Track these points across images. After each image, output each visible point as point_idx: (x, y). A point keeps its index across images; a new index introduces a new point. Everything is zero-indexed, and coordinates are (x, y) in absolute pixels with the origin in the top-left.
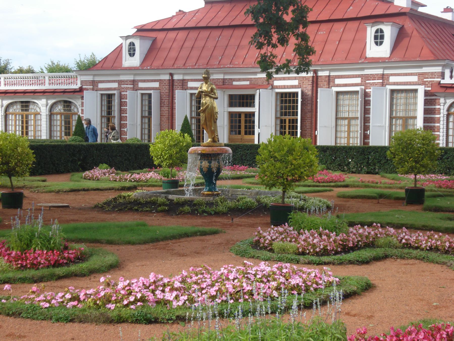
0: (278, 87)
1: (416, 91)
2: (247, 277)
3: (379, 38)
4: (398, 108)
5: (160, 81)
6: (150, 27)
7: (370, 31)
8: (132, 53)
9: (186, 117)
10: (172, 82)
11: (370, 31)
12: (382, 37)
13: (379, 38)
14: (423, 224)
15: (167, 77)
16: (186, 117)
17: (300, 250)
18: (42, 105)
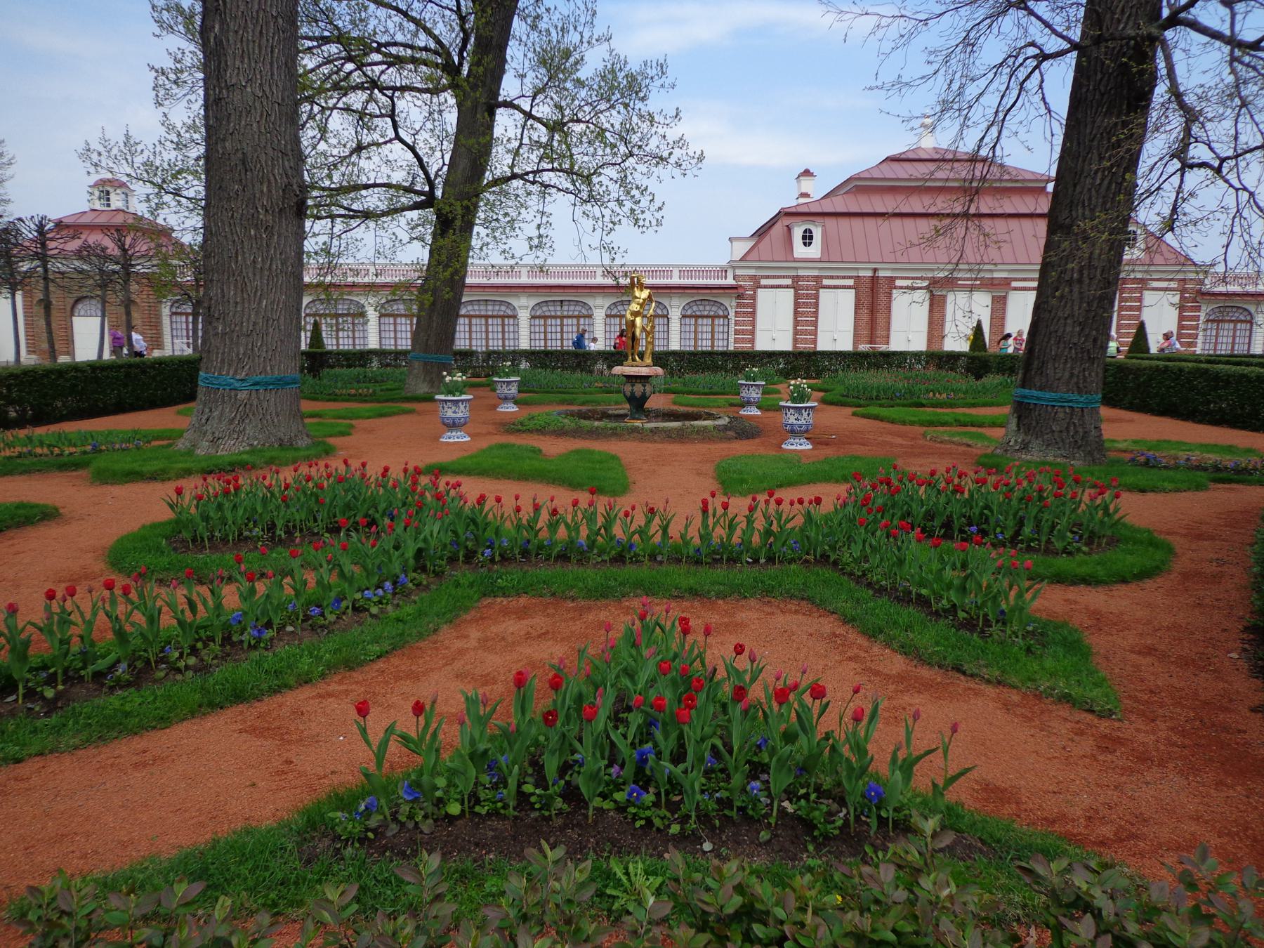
2: (179, 202)
3: (808, 239)
4: (184, 326)
5: (857, 278)
6: (794, 210)
7: (798, 233)
9: (978, 329)
10: (874, 280)
11: (798, 233)
12: (811, 238)
13: (808, 239)
14: (17, 500)
15: (870, 274)
16: (978, 329)
17: (21, 930)
18: (600, 307)
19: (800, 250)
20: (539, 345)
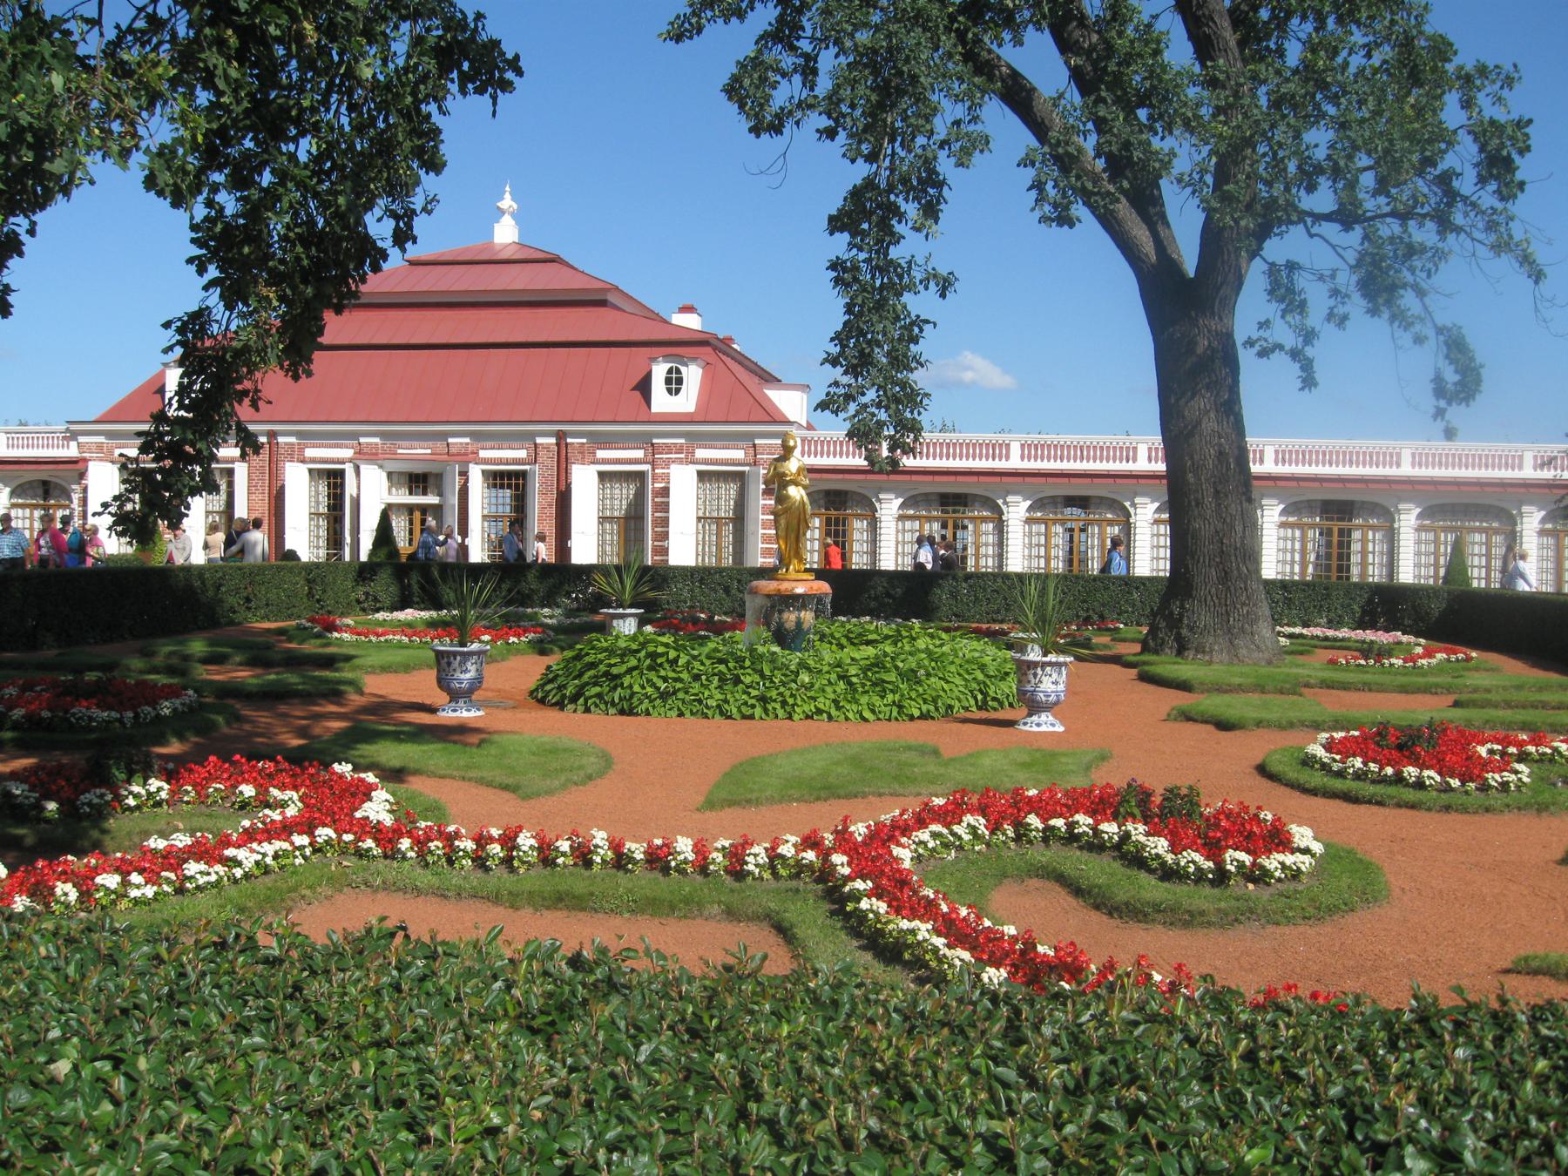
0: (313, 461)
1: (743, 473)
19: (661, 401)
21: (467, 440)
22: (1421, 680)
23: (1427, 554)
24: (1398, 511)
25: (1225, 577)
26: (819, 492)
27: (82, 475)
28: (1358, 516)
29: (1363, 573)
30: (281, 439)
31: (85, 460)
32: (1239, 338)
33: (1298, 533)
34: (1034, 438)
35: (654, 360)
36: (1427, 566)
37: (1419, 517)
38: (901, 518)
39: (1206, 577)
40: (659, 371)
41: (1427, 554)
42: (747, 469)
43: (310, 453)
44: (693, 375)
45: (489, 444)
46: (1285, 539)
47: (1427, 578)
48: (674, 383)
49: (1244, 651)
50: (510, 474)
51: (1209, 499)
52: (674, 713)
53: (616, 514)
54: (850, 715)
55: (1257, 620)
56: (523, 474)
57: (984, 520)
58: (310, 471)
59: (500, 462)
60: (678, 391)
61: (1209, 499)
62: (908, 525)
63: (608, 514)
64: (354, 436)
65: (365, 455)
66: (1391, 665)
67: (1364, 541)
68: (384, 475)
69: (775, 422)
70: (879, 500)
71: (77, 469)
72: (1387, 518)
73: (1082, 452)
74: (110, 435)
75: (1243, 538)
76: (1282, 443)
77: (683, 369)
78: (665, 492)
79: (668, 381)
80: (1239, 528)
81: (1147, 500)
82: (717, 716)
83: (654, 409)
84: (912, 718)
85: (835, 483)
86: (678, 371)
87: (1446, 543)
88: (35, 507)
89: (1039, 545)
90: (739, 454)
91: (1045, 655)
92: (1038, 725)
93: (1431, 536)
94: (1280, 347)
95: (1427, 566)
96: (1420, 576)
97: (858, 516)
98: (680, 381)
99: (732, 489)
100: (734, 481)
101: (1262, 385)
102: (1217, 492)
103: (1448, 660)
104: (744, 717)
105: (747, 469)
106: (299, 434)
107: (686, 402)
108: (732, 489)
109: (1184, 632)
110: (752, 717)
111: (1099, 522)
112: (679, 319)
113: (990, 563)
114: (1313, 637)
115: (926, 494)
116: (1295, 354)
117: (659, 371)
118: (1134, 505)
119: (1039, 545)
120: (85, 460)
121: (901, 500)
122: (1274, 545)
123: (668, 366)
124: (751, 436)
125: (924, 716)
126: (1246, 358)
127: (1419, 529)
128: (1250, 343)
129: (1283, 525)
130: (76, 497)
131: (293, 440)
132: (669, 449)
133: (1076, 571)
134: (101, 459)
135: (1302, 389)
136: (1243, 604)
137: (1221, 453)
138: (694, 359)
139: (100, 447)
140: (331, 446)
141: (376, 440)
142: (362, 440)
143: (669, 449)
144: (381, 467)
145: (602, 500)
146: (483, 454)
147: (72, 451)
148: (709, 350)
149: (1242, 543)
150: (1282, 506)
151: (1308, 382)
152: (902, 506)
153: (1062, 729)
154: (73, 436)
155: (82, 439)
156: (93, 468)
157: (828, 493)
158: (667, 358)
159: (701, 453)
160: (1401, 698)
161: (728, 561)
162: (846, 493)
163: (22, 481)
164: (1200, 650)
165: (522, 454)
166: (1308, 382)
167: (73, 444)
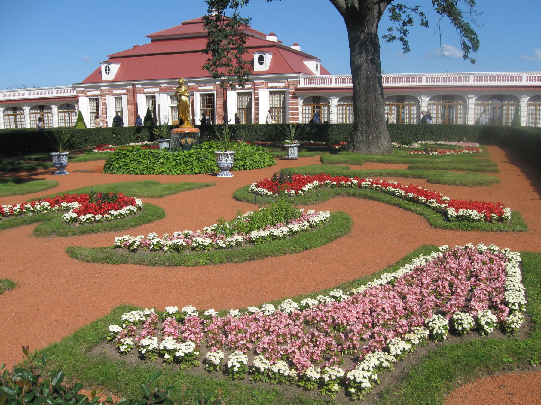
0: (147, 93)
1: (284, 91)
8: (108, 71)
20: (342, 121)
21: (194, 84)
22: (411, 159)
23: (532, 114)
24: (521, 98)
25: (368, 123)
26: (310, 97)
27: (78, 101)
28: (506, 100)
29: (507, 122)
30: (137, 86)
31: (78, 96)
32: (380, 35)
33: (482, 107)
34: (338, 76)
35: (254, 53)
36: (532, 119)
37: (529, 100)
38: (339, 105)
39: (362, 122)
40: (256, 57)
41: (532, 114)
42: (286, 90)
43: (146, 90)
44: (268, 58)
45: (201, 85)
46: (478, 109)
47: (532, 123)
48: (261, 61)
49: (373, 150)
50: (209, 95)
51: (363, 95)
52: (121, 173)
53: (244, 107)
54: (173, 173)
55: (380, 138)
56: (213, 95)
57: (413, 105)
58: (147, 96)
59: (205, 91)
60: (263, 63)
61: (363, 95)
62: (341, 107)
63: (241, 107)
64: (159, 84)
65: (162, 91)
66: (433, 154)
67: (508, 110)
68: (169, 97)
69: (295, 73)
70: (330, 99)
71: (75, 99)
72: (517, 100)
73: (405, 79)
74: (85, 88)
75: (375, 109)
76: (396, 72)
77: (264, 56)
78: (257, 99)
79: (259, 60)
80: (374, 105)
81: (426, 96)
82: (134, 174)
83: (255, 70)
84: (196, 174)
85: (315, 94)
86: (262, 57)
87: (512, 110)
88: (66, 112)
89: (343, 114)
90: (283, 85)
91: (226, 151)
92: (222, 175)
93: (534, 107)
94: (395, 38)
95: (532, 119)
96: (529, 123)
97: (323, 105)
98: (263, 60)
99: (282, 96)
100: (282, 94)
101: (389, 52)
102: (366, 92)
103: (469, 153)
104: (141, 174)
105: (286, 90)
106: (142, 84)
107: (265, 67)
108: (282, 96)
109: (355, 143)
110: (143, 174)
111: (409, 105)
112: (269, 38)
113: (415, 120)
114: (446, 145)
115: (347, 97)
116: (401, 39)
117: (256, 57)
118: (421, 98)
119: (343, 114)
120: (78, 96)
121: (338, 99)
122: (473, 112)
123: (259, 55)
124: (287, 78)
125: (200, 173)
126: (382, 42)
127: (529, 105)
128: (385, 37)
129: (476, 104)
130: (76, 108)
131: (140, 86)
132: (259, 84)
133: (400, 123)
134: (83, 96)
135: (404, 53)
136: (375, 132)
137: (367, 78)
138: (267, 52)
139: (83, 92)
140: (152, 88)
141: (166, 85)
142: (162, 85)
143: (259, 84)
144: (168, 94)
145: (239, 102)
146: (200, 88)
147: (74, 94)
148: (275, 48)
149: (375, 111)
150: (476, 98)
151: (407, 49)
152: (339, 101)
153: (232, 176)
154: (75, 89)
155: (77, 89)
156: (80, 99)
157: (313, 97)
158: (258, 52)
159: (270, 85)
160: (95, 162)
161: (281, 122)
162: (320, 97)
163: (61, 104)
164: (358, 150)
165: (212, 88)
166: (407, 49)
167: (75, 91)
